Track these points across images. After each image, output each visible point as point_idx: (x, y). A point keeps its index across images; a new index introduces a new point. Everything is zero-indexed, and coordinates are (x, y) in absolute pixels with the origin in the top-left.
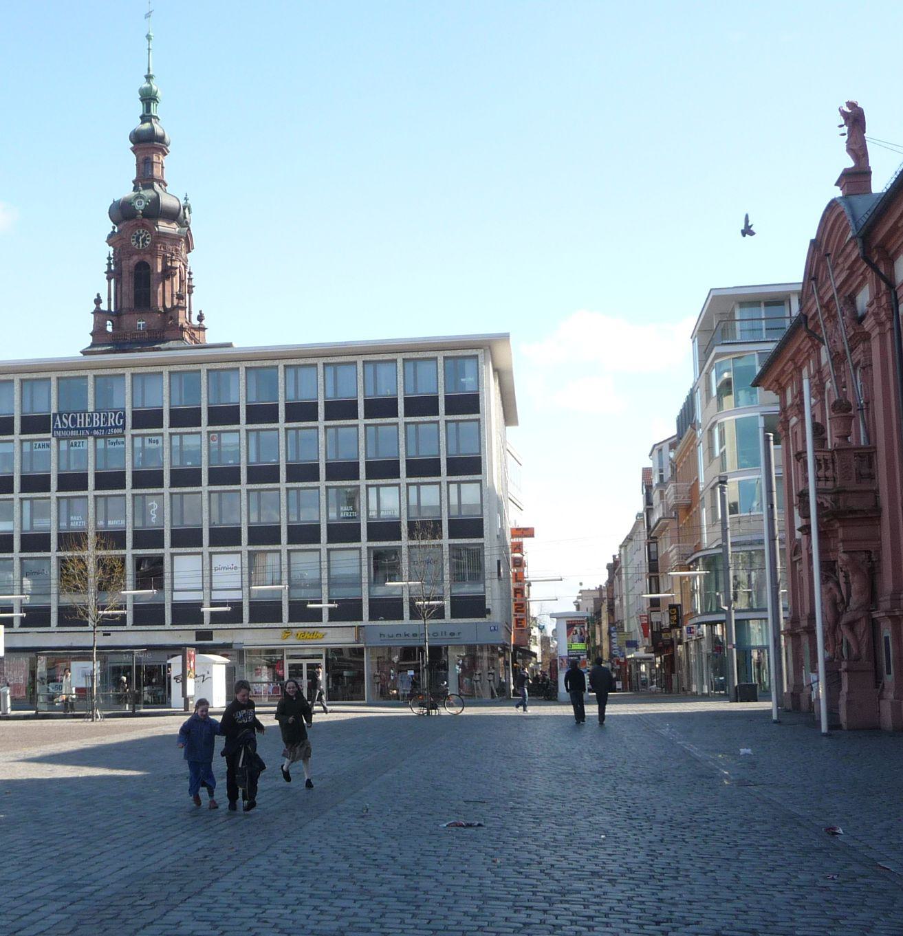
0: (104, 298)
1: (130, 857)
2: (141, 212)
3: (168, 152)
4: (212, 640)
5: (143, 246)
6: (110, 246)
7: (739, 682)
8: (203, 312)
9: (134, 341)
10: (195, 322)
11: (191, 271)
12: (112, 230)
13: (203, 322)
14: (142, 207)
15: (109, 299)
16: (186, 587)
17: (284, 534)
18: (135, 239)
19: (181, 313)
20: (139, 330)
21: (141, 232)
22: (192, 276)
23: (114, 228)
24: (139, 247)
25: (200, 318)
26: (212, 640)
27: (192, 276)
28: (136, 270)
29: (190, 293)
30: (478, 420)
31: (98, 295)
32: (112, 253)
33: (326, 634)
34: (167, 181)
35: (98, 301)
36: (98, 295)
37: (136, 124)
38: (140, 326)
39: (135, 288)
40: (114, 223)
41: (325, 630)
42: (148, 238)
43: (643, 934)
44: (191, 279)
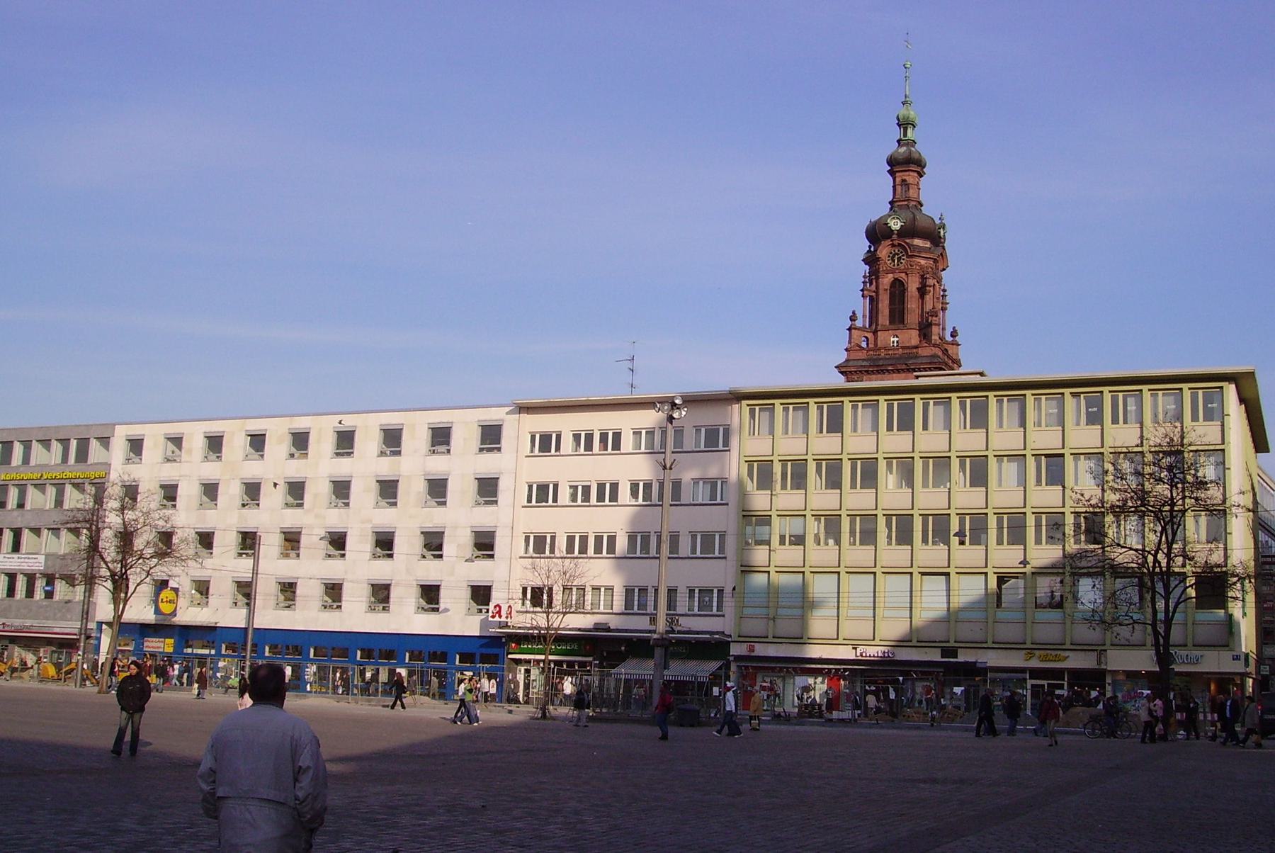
0: (859, 315)
1: (886, 832)
2: (896, 232)
3: (925, 174)
4: (957, 657)
5: (898, 265)
6: (866, 264)
7: (1181, 674)
8: (956, 329)
9: (887, 357)
10: (949, 338)
11: (946, 288)
12: (868, 249)
13: (957, 338)
14: (898, 227)
15: (864, 316)
16: (948, 379)
17: (839, 715)
18: (890, 261)
19: (935, 329)
20: (893, 346)
21: (897, 251)
22: (946, 293)
23: (870, 247)
24: (894, 265)
25: (954, 334)
26: (957, 657)
27: (946, 293)
28: (891, 287)
29: (944, 309)
30: (1223, 450)
31: (854, 312)
32: (868, 271)
33: (1068, 657)
34: (923, 202)
35: (853, 318)
36: (854, 312)
37: (891, 148)
38: (893, 342)
39: (890, 304)
40: (870, 242)
41: (1067, 653)
42: (903, 257)
43: (936, 642)
44: (946, 296)
